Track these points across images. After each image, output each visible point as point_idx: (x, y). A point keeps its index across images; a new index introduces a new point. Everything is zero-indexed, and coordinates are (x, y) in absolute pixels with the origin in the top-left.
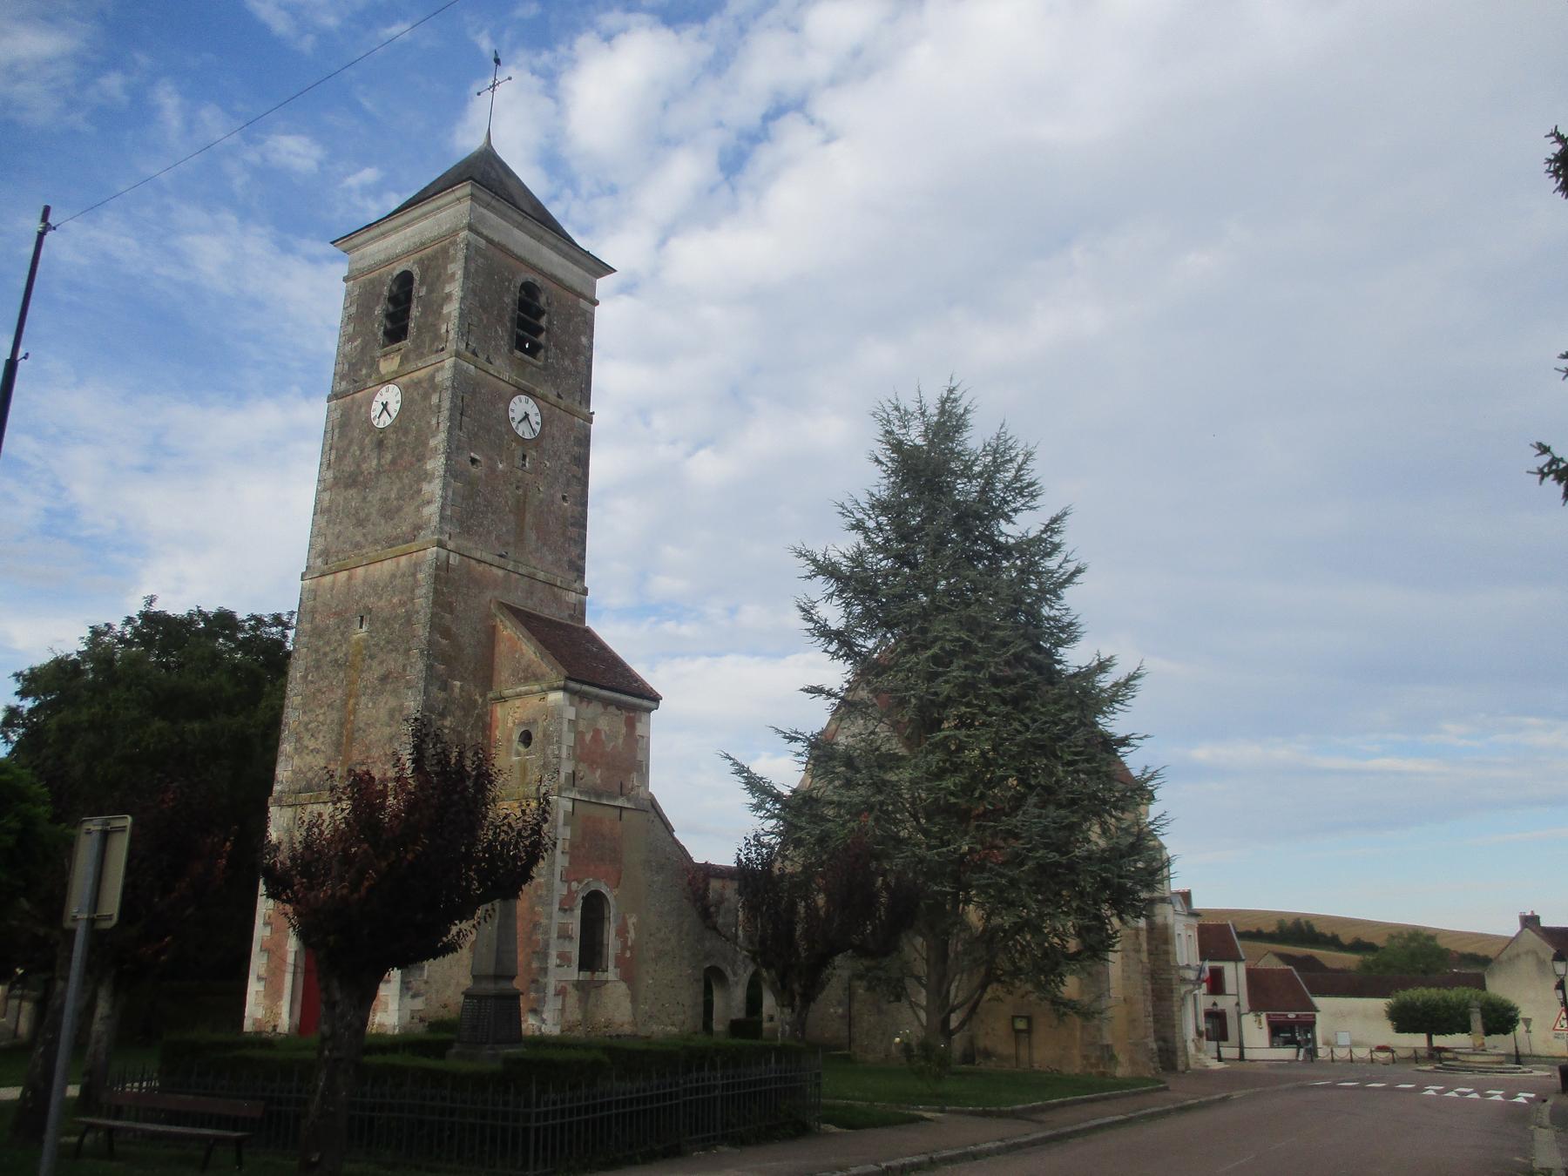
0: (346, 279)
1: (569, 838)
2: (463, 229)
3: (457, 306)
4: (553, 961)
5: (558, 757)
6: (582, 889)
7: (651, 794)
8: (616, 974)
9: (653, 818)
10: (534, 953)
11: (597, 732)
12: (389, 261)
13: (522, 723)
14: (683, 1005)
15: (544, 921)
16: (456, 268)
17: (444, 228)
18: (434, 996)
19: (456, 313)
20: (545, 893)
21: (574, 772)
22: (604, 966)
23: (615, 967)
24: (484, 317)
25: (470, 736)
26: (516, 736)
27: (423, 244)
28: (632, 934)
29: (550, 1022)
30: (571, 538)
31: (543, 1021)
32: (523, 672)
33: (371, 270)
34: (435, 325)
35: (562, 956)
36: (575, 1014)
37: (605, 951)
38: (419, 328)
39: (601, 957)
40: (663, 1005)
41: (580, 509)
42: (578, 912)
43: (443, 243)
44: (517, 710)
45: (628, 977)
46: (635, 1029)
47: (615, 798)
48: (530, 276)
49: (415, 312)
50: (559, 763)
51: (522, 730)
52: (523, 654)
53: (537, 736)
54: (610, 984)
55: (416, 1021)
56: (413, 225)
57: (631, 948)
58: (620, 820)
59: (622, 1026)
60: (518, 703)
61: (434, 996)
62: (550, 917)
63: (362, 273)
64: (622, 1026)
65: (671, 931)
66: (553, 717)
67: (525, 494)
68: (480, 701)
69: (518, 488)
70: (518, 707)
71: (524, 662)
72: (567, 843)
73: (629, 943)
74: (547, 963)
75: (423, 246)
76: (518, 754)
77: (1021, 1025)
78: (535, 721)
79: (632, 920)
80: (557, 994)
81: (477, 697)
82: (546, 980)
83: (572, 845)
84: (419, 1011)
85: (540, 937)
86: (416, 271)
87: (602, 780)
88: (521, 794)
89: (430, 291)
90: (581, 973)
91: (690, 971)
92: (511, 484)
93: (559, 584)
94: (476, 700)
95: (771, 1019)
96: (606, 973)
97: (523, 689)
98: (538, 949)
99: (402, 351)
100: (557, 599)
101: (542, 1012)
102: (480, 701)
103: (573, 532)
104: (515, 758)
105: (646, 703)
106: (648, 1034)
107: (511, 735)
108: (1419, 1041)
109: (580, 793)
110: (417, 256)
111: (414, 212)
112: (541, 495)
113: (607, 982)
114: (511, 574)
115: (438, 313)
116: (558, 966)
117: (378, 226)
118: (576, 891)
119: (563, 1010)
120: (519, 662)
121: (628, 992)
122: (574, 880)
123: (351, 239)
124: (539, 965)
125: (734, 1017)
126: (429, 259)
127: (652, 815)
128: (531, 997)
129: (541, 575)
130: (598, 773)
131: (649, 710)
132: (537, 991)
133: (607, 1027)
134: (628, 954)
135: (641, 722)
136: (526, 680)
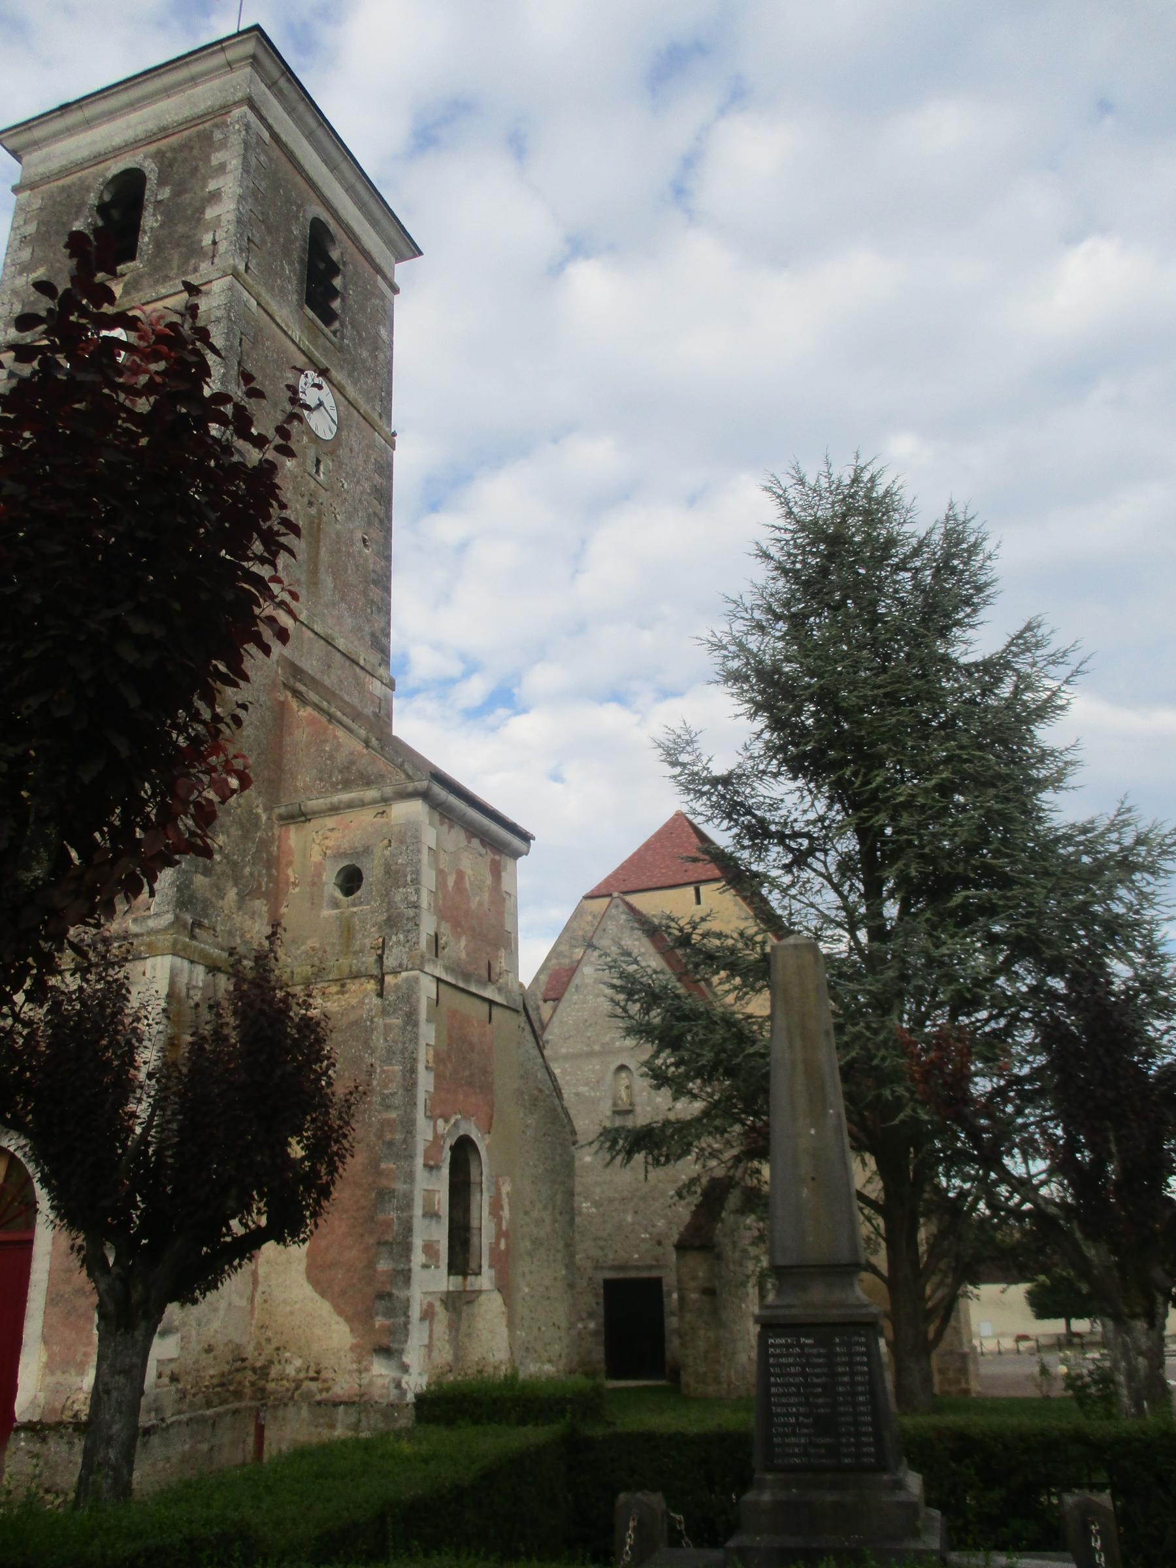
0: (16, 190)
1: (433, 1043)
2: (237, 104)
3: (232, 206)
4: (418, 1257)
5: (416, 906)
10: (379, 1243)
11: (460, 875)
12: (99, 158)
13: (339, 855)
15: (400, 1187)
16: (230, 157)
17: (203, 107)
18: (194, 1333)
19: (232, 217)
20: (398, 1137)
21: (436, 936)
24: (268, 239)
25: (251, 874)
26: (330, 878)
27: (164, 129)
28: (506, 1213)
29: (415, 1369)
30: (373, 602)
31: (405, 1369)
32: (341, 771)
33: (65, 172)
34: (188, 237)
35: (429, 1249)
36: (444, 1355)
37: (474, 1240)
38: (159, 245)
41: (383, 563)
42: (445, 1171)
43: (201, 127)
44: (329, 834)
45: (504, 1286)
48: (325, 216)
49: (150, 220)
50: (417, 916)
51: (338, 869)
52: (339, 745)
53: (372, 873)
55: (165, 1380)
56: (141, 108)
58: (490, 1021)
60: (330, 822)
61: (194, 1333)
62: (410, 1177)
63: (47, 178)
66: (402, 842)
67: (320, 513)
68: (264, 817)
69: (311, 504)
70: (332, 830)
71: (341, 758)
72: (431, 1052)
74: (409, 1261)
75: (164, 132)
76: (336, 904)
78: (367, 850)
79: (506, 1188)
80: (422, 1319)
81: (260, 811)
82: (407, 1293)
83: (437, 1055)
84: (171, 1360)
85: (393, 1215)
86: (151, 169)
87: (468, 954)
88: (346, 970)
89: (176, 194)
90: (452, 1278)
92: (303, 496)
93: (362, 662)
94: (258, 817)
97: (345, 797)
98: (389, 1238)
99: (126, 278)
100: (360, 685)
101: (401, 1352)
102: (264, 817)
103: (375, 593)
104: (327, 912)
105: (516, 842)
107: (320, 876)
108: (1056, 1326)
109: (447, 969)
110: (153, 148)
111: (149, 83)
112: (338, 526)
113: (480, 1292)
114: (304, 629)
115: (196, 217)
116: (425, 1266)
117: (81, 107)
119: (429, 1347)
120: (331, 757)
121: (504, 1309)
123: (30, 128)
124: (391, 1266)
126: (173, 150)
128: (377, 1325)
129: (341, 643)
130: (463, 943)
131: (516, 854)
132: (390, 1313)
136: (347, 785)
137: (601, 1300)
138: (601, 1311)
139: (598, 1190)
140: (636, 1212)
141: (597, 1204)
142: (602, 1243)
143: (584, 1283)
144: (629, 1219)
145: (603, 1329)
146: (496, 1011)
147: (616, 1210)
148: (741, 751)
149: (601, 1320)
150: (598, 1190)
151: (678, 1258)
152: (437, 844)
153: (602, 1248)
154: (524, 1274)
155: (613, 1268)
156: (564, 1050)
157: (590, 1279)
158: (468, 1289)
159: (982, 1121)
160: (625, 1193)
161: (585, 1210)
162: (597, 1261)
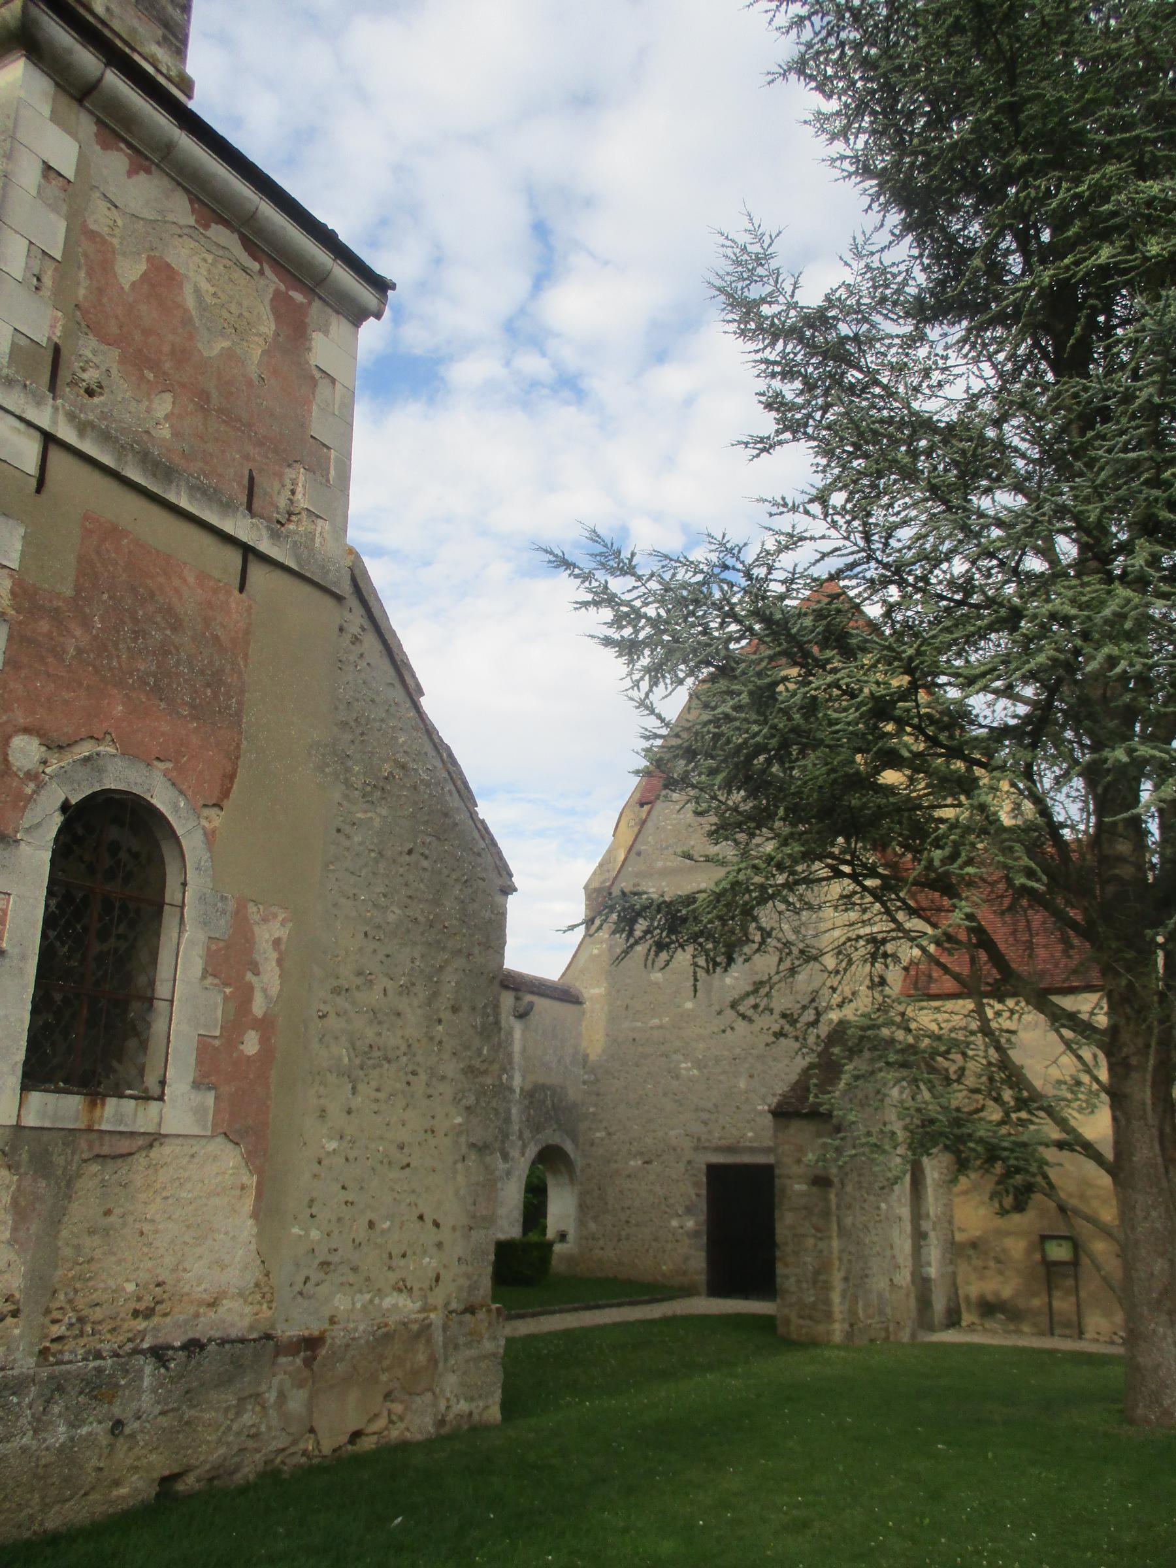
6: (62, 776)
7: (351, 551)
8: (199, 1111)
9: (355, 630)
14: (437, 1225)
22: (151, 1081)
23: (197, 1085)
39: (144, 1045)
40: (371, 1224)
46: (266, 1313)
47: (227, 507)
54: (167, 1150)
57: (265, 1025)
58: (242, 589)
59: (213, 1304)
64: (213, 1304)
65: (406, 990)
73: (258, 1007)
77: (1059, 1252)
90: (35, 1097)
91: (459, 1120)
95: (563, 1237)
96: (154, 1106)
105: (366, 295)
106: (314, 1328)
113: (155, 1139)
118: (31, 776)
122: (26, 730)
125: (502, 1236)
127: (356, 619)
131: (358, 315)
133: (149, 1313)
134: (251, 1044)
135: (326, 333)
137: (704, 1192)
138: (703, 1205)
139: (702, 1045)
140: (751, 1076)
141: (699, 1064)
142: (705, 1116)
143: (681, 1167)
144: (742, 1085)
145: (704, 1228)
146: (258, 574)
147: (724, 1072)
148: (848, 257)
149: (703, 1217)
150: (702, 1045)
151: (777, 1130)
152: (78, 172)
153: (705, 1123)
154: (323, 1114)
155: (718, 1149)
156: (660, 864)
157: (689, 1162)
158: (162, 1132)
159: (940, 1446)
160: (738, 1051)
161: (683, 1072)
162: (699, 1139)
